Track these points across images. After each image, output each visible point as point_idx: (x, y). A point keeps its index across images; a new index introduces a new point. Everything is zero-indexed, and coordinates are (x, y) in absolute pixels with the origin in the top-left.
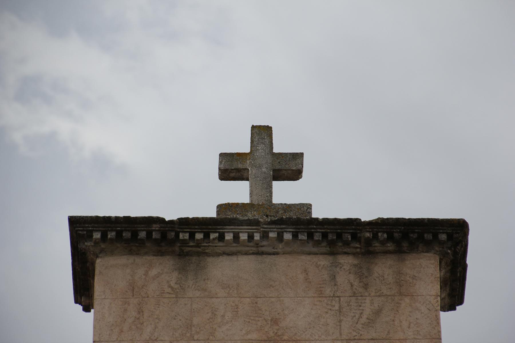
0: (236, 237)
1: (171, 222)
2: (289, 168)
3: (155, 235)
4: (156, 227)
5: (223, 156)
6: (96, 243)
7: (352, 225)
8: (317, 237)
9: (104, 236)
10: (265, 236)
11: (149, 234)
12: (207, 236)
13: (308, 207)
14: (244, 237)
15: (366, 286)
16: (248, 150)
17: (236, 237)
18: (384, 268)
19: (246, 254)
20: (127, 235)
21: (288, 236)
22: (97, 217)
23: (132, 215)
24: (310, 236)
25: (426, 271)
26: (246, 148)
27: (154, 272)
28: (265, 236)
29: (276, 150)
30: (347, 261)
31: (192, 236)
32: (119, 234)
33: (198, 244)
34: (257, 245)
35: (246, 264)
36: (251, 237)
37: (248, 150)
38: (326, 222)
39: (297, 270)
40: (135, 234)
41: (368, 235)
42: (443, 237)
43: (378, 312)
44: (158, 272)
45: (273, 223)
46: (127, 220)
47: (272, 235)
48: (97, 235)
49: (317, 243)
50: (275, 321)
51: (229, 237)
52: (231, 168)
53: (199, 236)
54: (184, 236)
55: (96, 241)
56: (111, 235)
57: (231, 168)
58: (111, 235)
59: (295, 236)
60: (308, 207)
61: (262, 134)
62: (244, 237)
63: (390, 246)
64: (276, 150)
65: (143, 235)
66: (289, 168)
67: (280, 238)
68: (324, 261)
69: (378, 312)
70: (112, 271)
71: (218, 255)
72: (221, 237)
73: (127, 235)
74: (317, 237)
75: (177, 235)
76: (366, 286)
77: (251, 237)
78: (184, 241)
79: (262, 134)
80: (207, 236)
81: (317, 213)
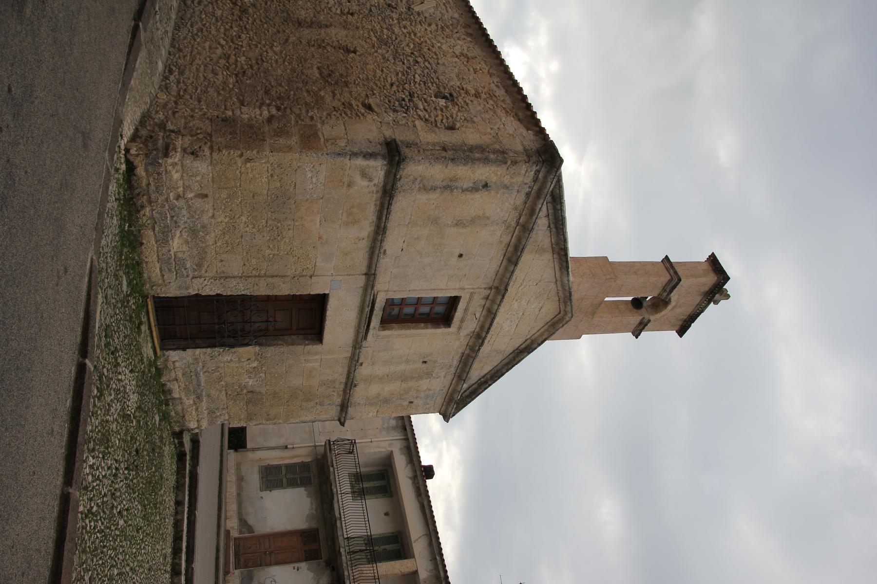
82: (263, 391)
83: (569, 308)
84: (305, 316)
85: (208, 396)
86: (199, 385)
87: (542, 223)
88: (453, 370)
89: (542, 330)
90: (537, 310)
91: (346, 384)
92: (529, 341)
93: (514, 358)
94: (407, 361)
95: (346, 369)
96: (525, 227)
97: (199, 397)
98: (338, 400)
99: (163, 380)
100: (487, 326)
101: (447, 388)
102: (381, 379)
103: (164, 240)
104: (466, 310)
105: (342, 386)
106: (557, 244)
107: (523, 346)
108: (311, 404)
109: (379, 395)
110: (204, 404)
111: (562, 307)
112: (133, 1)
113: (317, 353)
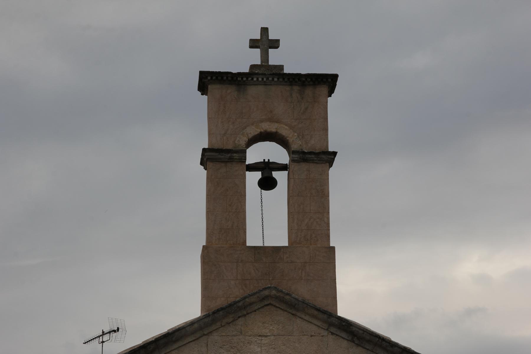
0: (258, 79)
1: (235, 74)
2: (275, 44)
3: (229, 78)
4: (229, 75)
5: (251, 40)
6: (209, 80)
7: (299, 75)
8: (286, 80)
9: (212, 78)
10: (268, 79)
11: (227, 78)
12: (247, 78)
13: (281, 67)
14: (260, 79)
15: (302, 98)
16: (259, 38)
17: (258, 79)
18: (309, 91)
19: (261, 85)
20: (219, 78)
21: (276, 79)
22: (209, 72)
23: (222, 71)
24: (284, 79)
25: (324, 89)
26: (258, 37)
27: (229, 91)
28: (268, 79)
29: (270, 38)
30: (296, 88)
31: (242, 78)
32: (217, 78)
33: (244, 81)
34: (265, 82)
35: (261, 89)
36: (263, 79)
37: (259, 38)
38: (289, 74)
39: (279, 91)
40: (222, 78)
41: (304, 79)
42: (330, 80)
43: (306, 109)
44: (230, 91)
45: (270, 74)
46: (220, 73)
47: (270, 79)
48: (209, 78)
49: (286, 82)
50: (271, 112)
51: (255, 79)
52: (254, 44)
53: (245, 79)
54: (239, 79)
55: (208, 81)
56: (214, 78)
57: (254, 44)
58: (214, 78)
59: (278, 79)
60: (281, 67)
61: (265, 31)
62: (260, 79)
63: (311, 83)
64: (270, 38)
65: (225, 78)
66: (275, 44)
67: (273, 79)
68: (288, 88)
69: (306, 109)
70: (214, 88)
71: (251, 85)
72: (253, 79)
73: (219, 78)
74: (286, 80)
75: (237, 79)
76: (302, 98)
77: (263, 79)
78: (240, 81)
79: (265, 31)
80: (247, 78)
81: (286, 71)
83: (253, 299)
89: (307, 318)
90: (265, 341)
92: (333, 329)
93: (369, 341)
107: (344, 335)
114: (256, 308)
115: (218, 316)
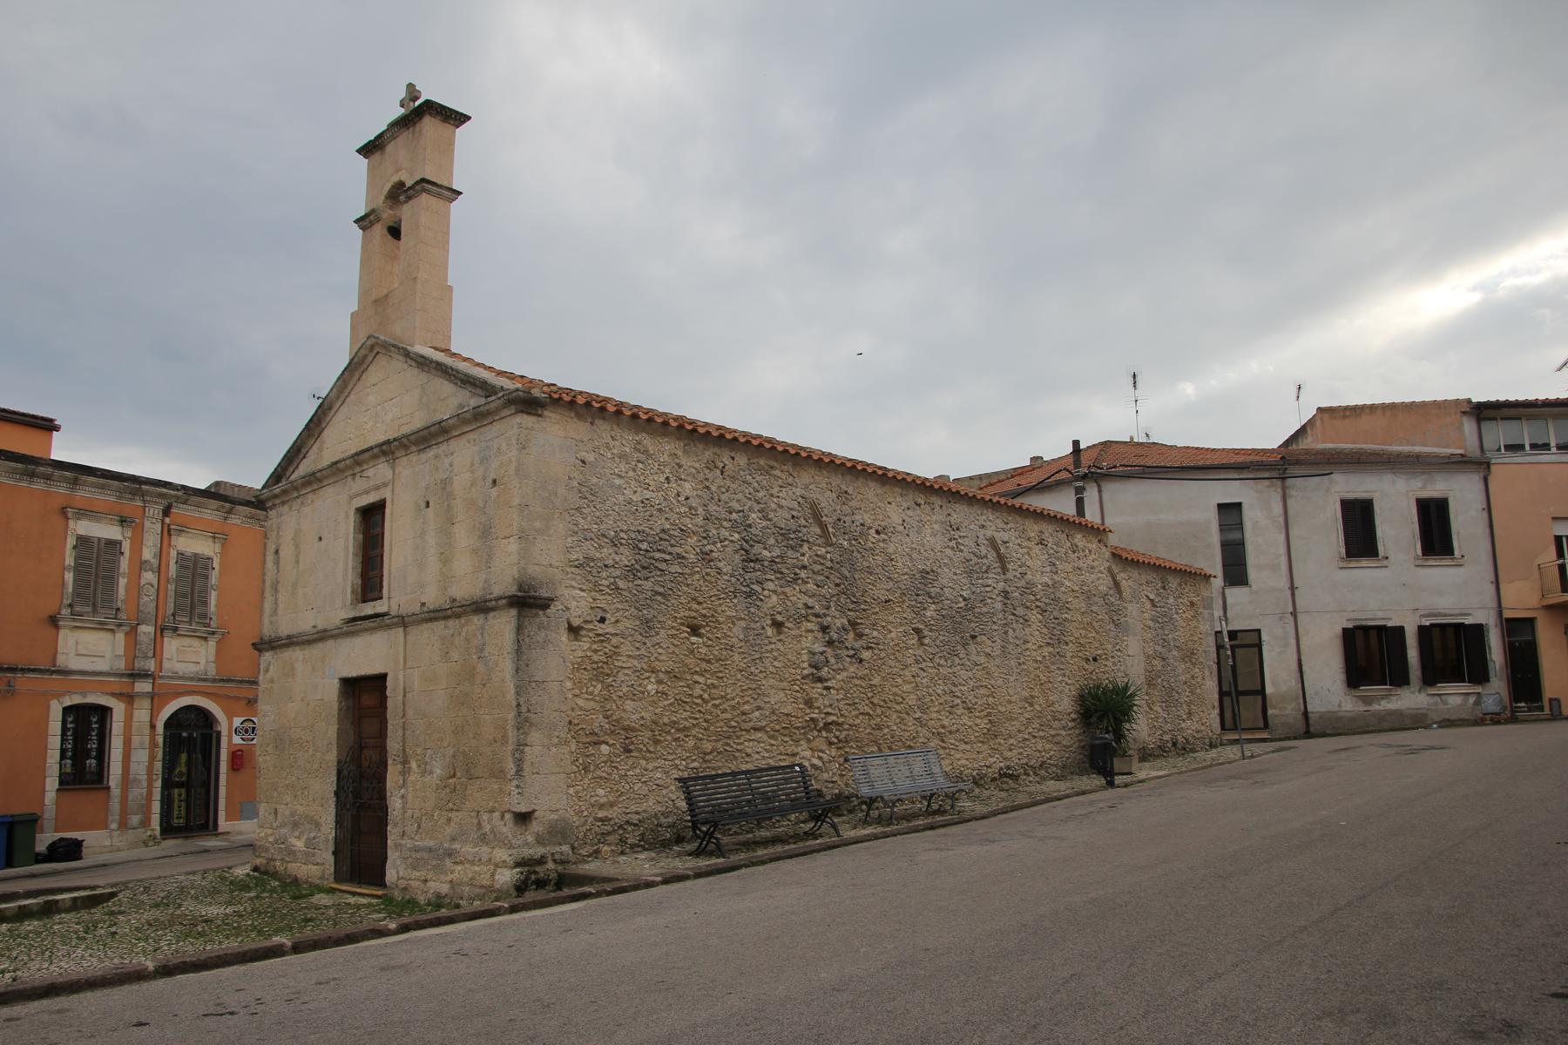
82: (451, 751)
83: (363, 352)
84: (365, 696)
85: (453, 839)
86: (430, 850)
87: (304, 468)
88: (444, 447)
91: (446, 618)
94: (422, 535)
95: (425, 626)
96: (315, 480)
97: (450, 854)
98: (477, 620)
99: (422, 900)
100: (367, 455)
101: (471, 436)
102: (445, 560)
103: (291, 852)
104: (367, 492)
105: (451, 623)
106: (310, 436)
108: (481, 668)
109: (475, 551)
110: (468, 849)
111: (370, 358)
112: (1565, 991)
113: (397, 679)
114: (136, 740)
115: (355, 369)
